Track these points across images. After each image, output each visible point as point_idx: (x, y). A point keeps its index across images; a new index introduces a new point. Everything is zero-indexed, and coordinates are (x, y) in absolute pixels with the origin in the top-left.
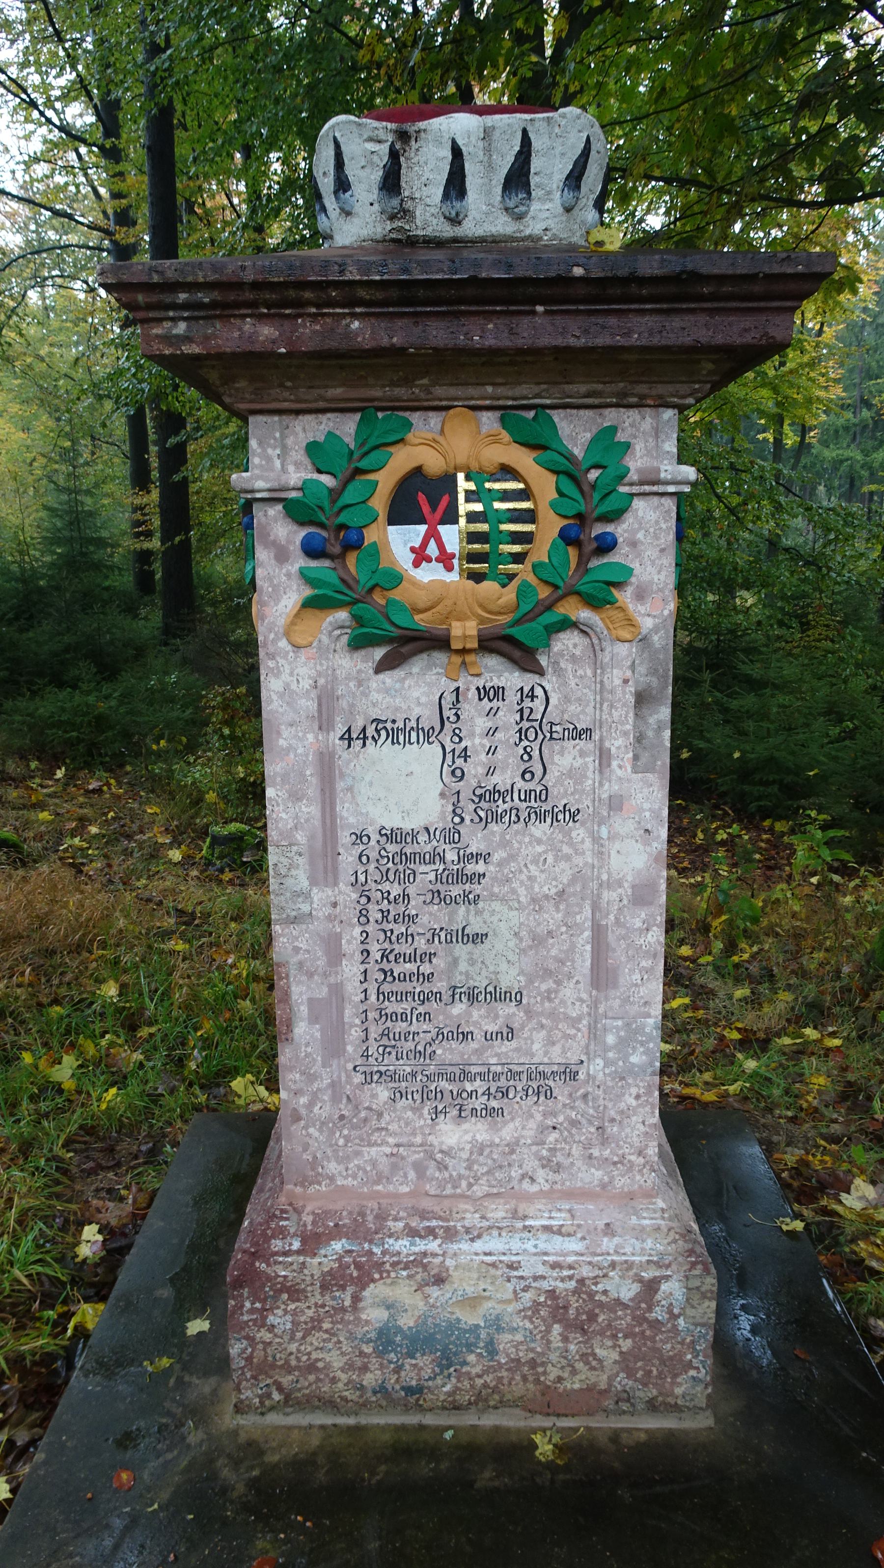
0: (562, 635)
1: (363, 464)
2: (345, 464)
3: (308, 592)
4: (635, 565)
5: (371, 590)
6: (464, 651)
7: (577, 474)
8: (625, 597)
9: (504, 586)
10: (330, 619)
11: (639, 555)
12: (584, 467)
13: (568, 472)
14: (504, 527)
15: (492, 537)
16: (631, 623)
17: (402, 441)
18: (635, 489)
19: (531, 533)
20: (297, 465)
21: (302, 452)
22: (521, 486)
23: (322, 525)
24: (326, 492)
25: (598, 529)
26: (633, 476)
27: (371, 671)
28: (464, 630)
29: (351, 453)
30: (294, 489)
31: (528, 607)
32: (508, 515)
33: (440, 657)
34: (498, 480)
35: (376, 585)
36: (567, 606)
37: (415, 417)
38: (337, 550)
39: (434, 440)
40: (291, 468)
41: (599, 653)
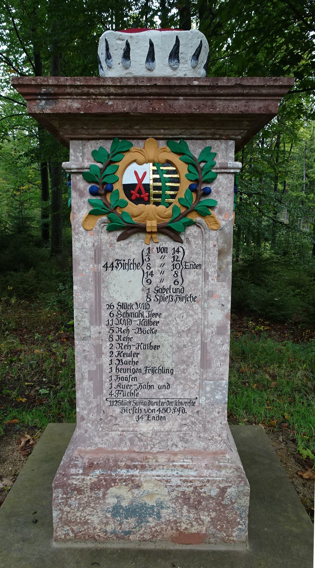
6: (151, 233)
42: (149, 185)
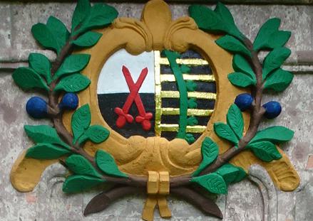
0: (237, 187)
1: (79, 42)
2: (63, 40)
3: (31, 146)
4: (295, 129)
5: (83, 144)
6: (157, 197)
7: (250, 54)
8: (288, 154)
9: (191, 143)
10: (49, 168)
12: (256, 48)
13: (243, 53)
14: (191, 94)
16: (292, 176)
17: (109, 26)
18: (295, 68)
19: (213, 101)
20: (24, 44)
21: (29, 33)
22: (205, 63)
23: (43, 91)
25: (267, 100)
26: (294, 57)
29: (69, 34)
30: (21, 61)
31: (210, 160)
32: (195, 85)
33: (138, 203)
34: (187, 58)
35: (88, 140)
37: (121, 8)
38: (55, 110)
39: (137, 24)
40: (19, 46)
42: (152, 96)
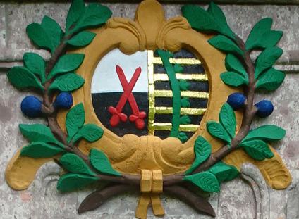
0: (229, 185)
1: (73, 41)
2: (58, 40)
3: (26, 144)
4: (287, 128)
5: (77, 143)
6: (151, 195)
7: (242, 53)
8: (280, 153)
9: (183, 141)
10: (43, 166)
11: (290, 121)
12: (247, 48)
13: (236, 53)
14: (184, 94)
15: (175, 100)
16: (284, 174)
17: (103, 25)
18: (287, 68)
19: (205, 100)
20: (19, 43)
21: (23, 33)
22: (198, 62)
23: (38, 91)
24: (42, 64)
25: (259, 99)
26: (285, 56)
27: (75, 212)
28: (152, 176)
29: (63, 34)
30: (16, 61)
31: (203, 158)
32: (187, 84)
33: (131, 201)
34: (180, 57)
35: (82, 139)
36: (234, 159)
37: (114, 8)
38: (50, 109)
39: (130, 24)
40: (14, 46)
41: (258, 199)
